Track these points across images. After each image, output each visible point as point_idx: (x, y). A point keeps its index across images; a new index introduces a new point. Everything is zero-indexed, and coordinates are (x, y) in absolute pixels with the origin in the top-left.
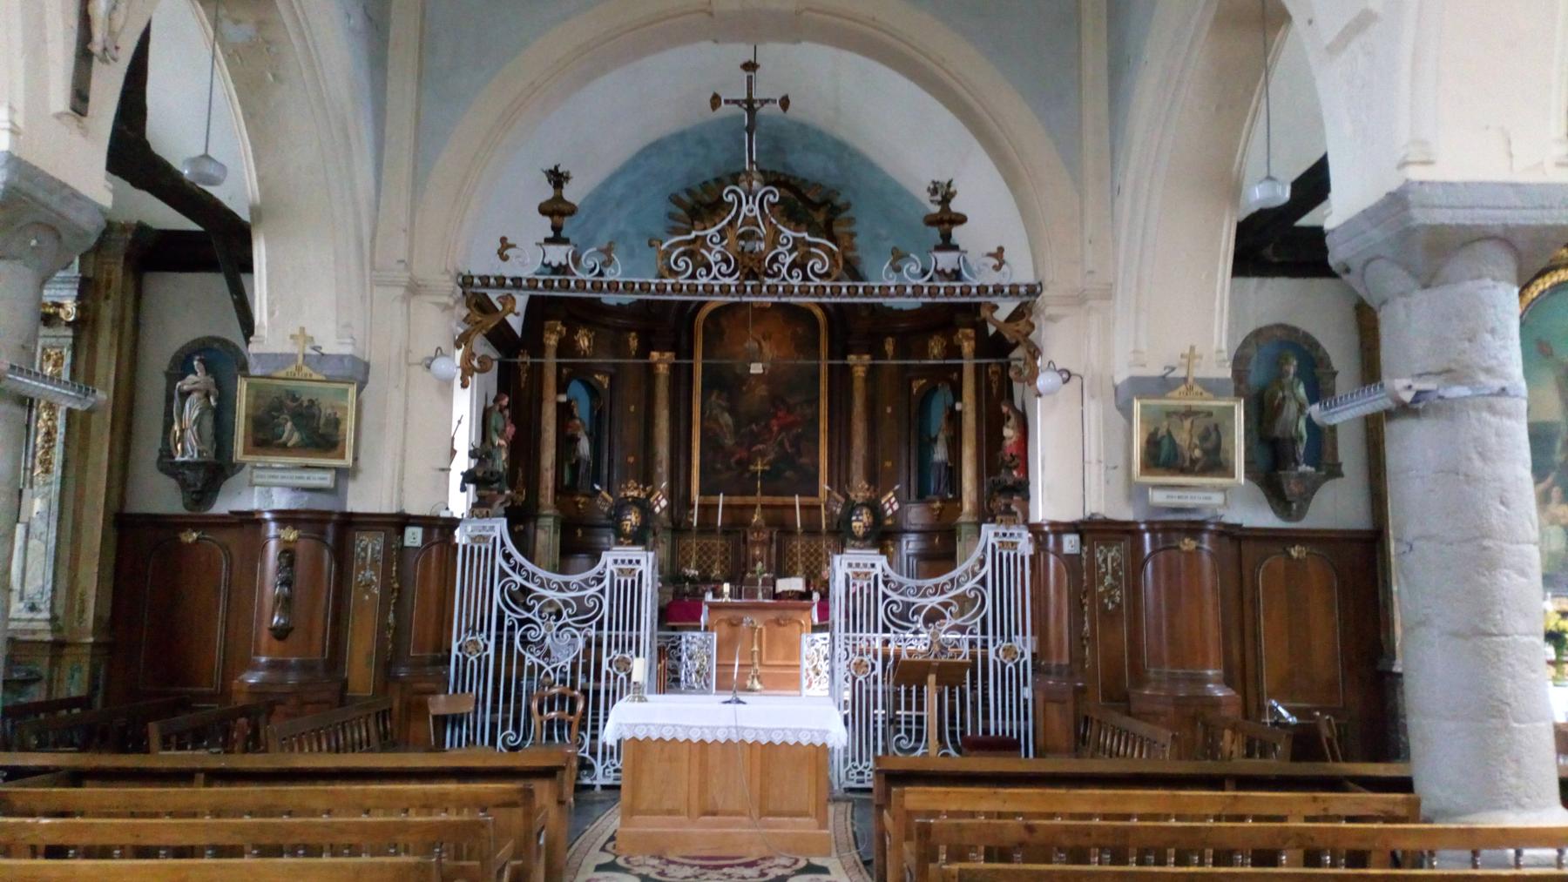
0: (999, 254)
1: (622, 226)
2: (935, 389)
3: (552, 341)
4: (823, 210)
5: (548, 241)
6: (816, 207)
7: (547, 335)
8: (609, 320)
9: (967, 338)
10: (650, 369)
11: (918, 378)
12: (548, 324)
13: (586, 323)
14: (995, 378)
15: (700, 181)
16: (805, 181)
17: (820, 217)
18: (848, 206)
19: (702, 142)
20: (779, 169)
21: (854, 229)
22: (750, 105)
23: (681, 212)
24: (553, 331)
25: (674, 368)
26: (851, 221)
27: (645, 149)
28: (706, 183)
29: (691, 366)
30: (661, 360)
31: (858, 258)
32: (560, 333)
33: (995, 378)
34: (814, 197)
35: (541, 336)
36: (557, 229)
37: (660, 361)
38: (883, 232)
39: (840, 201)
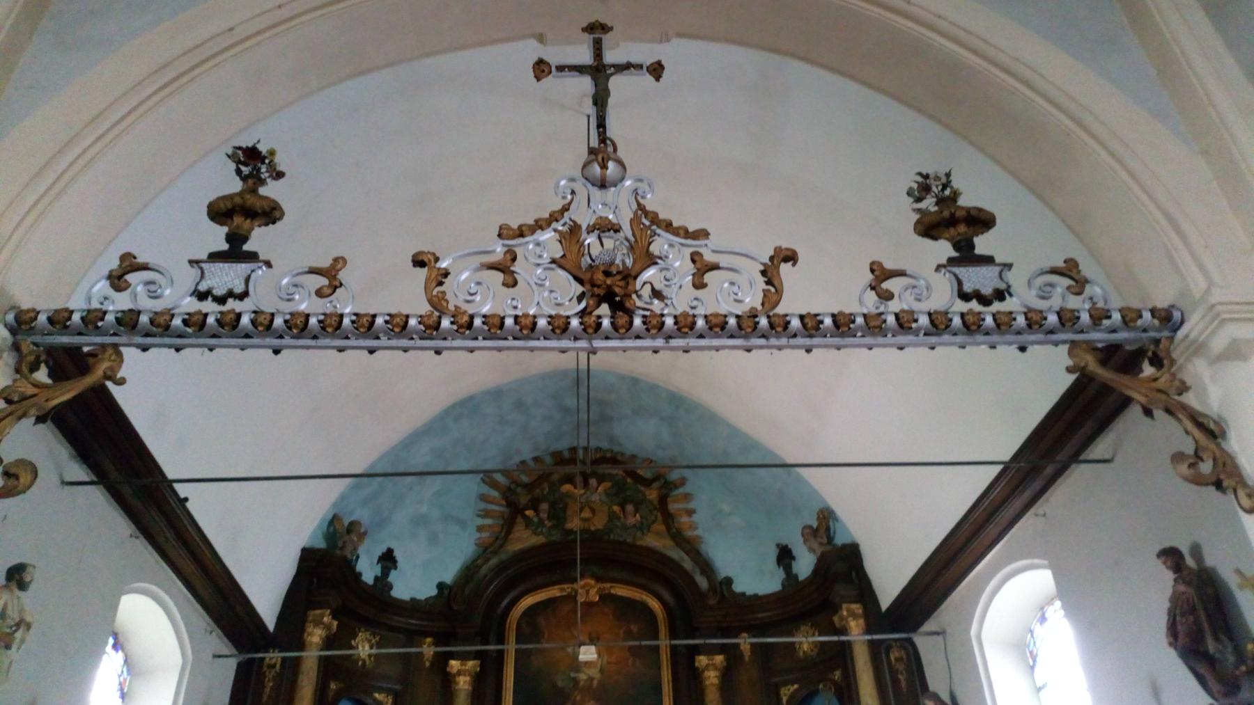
0: (1069, 270)
1: (424, 509)
2: (814, 693)
3: (315, 636)
4: (656, 485)
5: (215, 257)
6: (648, 483)
7: (310, 628)
8: (400, 621)
9: (854, 616)
10: (448, 681)
11: (785, 684)
12: (314, 614)
13: (370, 623)
14: (901, 667)
15: (517, 459)
16: (634, 457)
17: (652, 495)
18: (683, 481)
19: (520, 405)
20: (605, 445)
21: (691, 506)
22: (599, 71)
23: (495, 494)
24: (318, 623)
25: (478, 680)
26: (687, 497)
27: (454, 406)
28: (523, 462)
29: (501, 654)
30: (463, 672)
31: (699, 537)
32: (328, 627)
33: (901, 667)
34: (647, 473)
35: (303, 630)
36: (236, 240)
37: (459, 673)
38: (726, 508)
39: (674, 476)
